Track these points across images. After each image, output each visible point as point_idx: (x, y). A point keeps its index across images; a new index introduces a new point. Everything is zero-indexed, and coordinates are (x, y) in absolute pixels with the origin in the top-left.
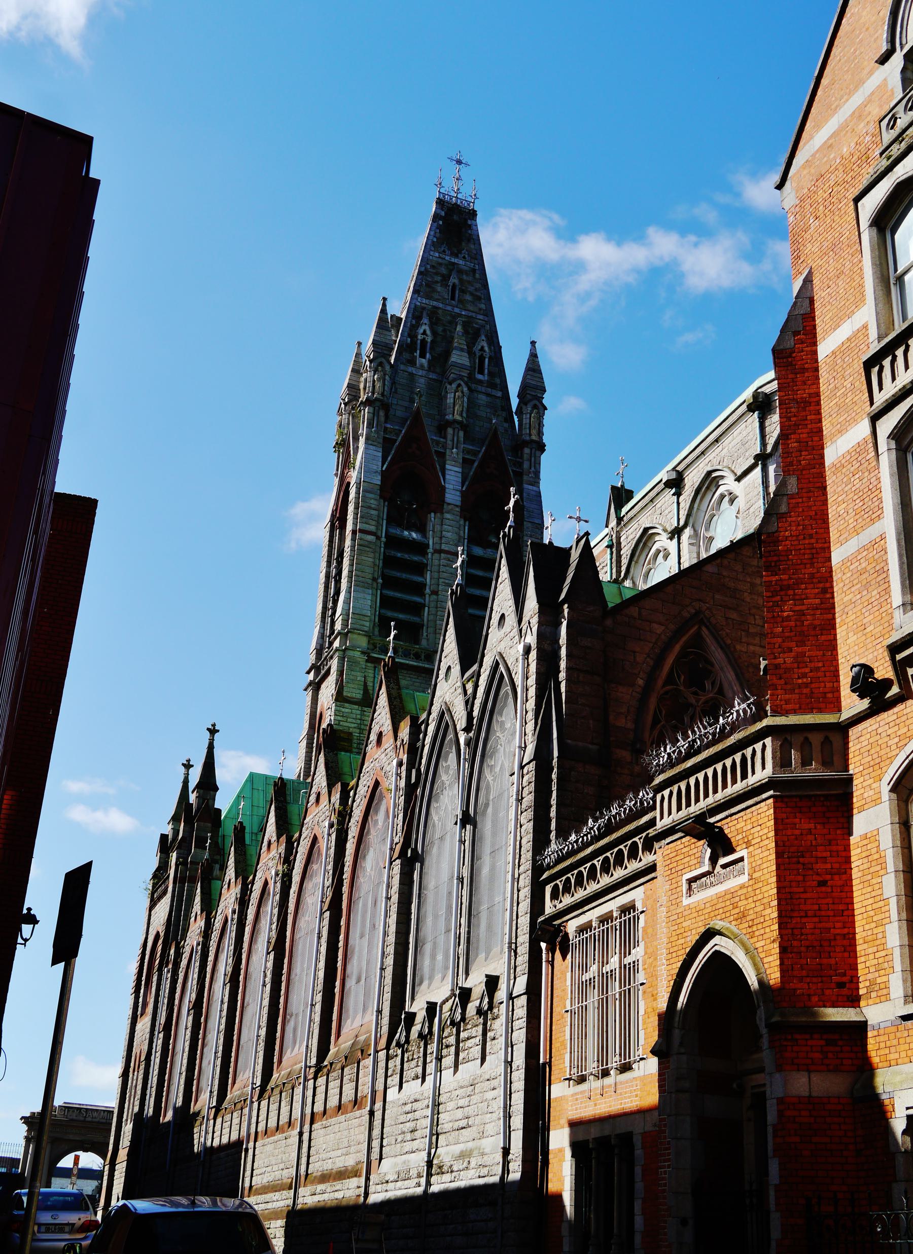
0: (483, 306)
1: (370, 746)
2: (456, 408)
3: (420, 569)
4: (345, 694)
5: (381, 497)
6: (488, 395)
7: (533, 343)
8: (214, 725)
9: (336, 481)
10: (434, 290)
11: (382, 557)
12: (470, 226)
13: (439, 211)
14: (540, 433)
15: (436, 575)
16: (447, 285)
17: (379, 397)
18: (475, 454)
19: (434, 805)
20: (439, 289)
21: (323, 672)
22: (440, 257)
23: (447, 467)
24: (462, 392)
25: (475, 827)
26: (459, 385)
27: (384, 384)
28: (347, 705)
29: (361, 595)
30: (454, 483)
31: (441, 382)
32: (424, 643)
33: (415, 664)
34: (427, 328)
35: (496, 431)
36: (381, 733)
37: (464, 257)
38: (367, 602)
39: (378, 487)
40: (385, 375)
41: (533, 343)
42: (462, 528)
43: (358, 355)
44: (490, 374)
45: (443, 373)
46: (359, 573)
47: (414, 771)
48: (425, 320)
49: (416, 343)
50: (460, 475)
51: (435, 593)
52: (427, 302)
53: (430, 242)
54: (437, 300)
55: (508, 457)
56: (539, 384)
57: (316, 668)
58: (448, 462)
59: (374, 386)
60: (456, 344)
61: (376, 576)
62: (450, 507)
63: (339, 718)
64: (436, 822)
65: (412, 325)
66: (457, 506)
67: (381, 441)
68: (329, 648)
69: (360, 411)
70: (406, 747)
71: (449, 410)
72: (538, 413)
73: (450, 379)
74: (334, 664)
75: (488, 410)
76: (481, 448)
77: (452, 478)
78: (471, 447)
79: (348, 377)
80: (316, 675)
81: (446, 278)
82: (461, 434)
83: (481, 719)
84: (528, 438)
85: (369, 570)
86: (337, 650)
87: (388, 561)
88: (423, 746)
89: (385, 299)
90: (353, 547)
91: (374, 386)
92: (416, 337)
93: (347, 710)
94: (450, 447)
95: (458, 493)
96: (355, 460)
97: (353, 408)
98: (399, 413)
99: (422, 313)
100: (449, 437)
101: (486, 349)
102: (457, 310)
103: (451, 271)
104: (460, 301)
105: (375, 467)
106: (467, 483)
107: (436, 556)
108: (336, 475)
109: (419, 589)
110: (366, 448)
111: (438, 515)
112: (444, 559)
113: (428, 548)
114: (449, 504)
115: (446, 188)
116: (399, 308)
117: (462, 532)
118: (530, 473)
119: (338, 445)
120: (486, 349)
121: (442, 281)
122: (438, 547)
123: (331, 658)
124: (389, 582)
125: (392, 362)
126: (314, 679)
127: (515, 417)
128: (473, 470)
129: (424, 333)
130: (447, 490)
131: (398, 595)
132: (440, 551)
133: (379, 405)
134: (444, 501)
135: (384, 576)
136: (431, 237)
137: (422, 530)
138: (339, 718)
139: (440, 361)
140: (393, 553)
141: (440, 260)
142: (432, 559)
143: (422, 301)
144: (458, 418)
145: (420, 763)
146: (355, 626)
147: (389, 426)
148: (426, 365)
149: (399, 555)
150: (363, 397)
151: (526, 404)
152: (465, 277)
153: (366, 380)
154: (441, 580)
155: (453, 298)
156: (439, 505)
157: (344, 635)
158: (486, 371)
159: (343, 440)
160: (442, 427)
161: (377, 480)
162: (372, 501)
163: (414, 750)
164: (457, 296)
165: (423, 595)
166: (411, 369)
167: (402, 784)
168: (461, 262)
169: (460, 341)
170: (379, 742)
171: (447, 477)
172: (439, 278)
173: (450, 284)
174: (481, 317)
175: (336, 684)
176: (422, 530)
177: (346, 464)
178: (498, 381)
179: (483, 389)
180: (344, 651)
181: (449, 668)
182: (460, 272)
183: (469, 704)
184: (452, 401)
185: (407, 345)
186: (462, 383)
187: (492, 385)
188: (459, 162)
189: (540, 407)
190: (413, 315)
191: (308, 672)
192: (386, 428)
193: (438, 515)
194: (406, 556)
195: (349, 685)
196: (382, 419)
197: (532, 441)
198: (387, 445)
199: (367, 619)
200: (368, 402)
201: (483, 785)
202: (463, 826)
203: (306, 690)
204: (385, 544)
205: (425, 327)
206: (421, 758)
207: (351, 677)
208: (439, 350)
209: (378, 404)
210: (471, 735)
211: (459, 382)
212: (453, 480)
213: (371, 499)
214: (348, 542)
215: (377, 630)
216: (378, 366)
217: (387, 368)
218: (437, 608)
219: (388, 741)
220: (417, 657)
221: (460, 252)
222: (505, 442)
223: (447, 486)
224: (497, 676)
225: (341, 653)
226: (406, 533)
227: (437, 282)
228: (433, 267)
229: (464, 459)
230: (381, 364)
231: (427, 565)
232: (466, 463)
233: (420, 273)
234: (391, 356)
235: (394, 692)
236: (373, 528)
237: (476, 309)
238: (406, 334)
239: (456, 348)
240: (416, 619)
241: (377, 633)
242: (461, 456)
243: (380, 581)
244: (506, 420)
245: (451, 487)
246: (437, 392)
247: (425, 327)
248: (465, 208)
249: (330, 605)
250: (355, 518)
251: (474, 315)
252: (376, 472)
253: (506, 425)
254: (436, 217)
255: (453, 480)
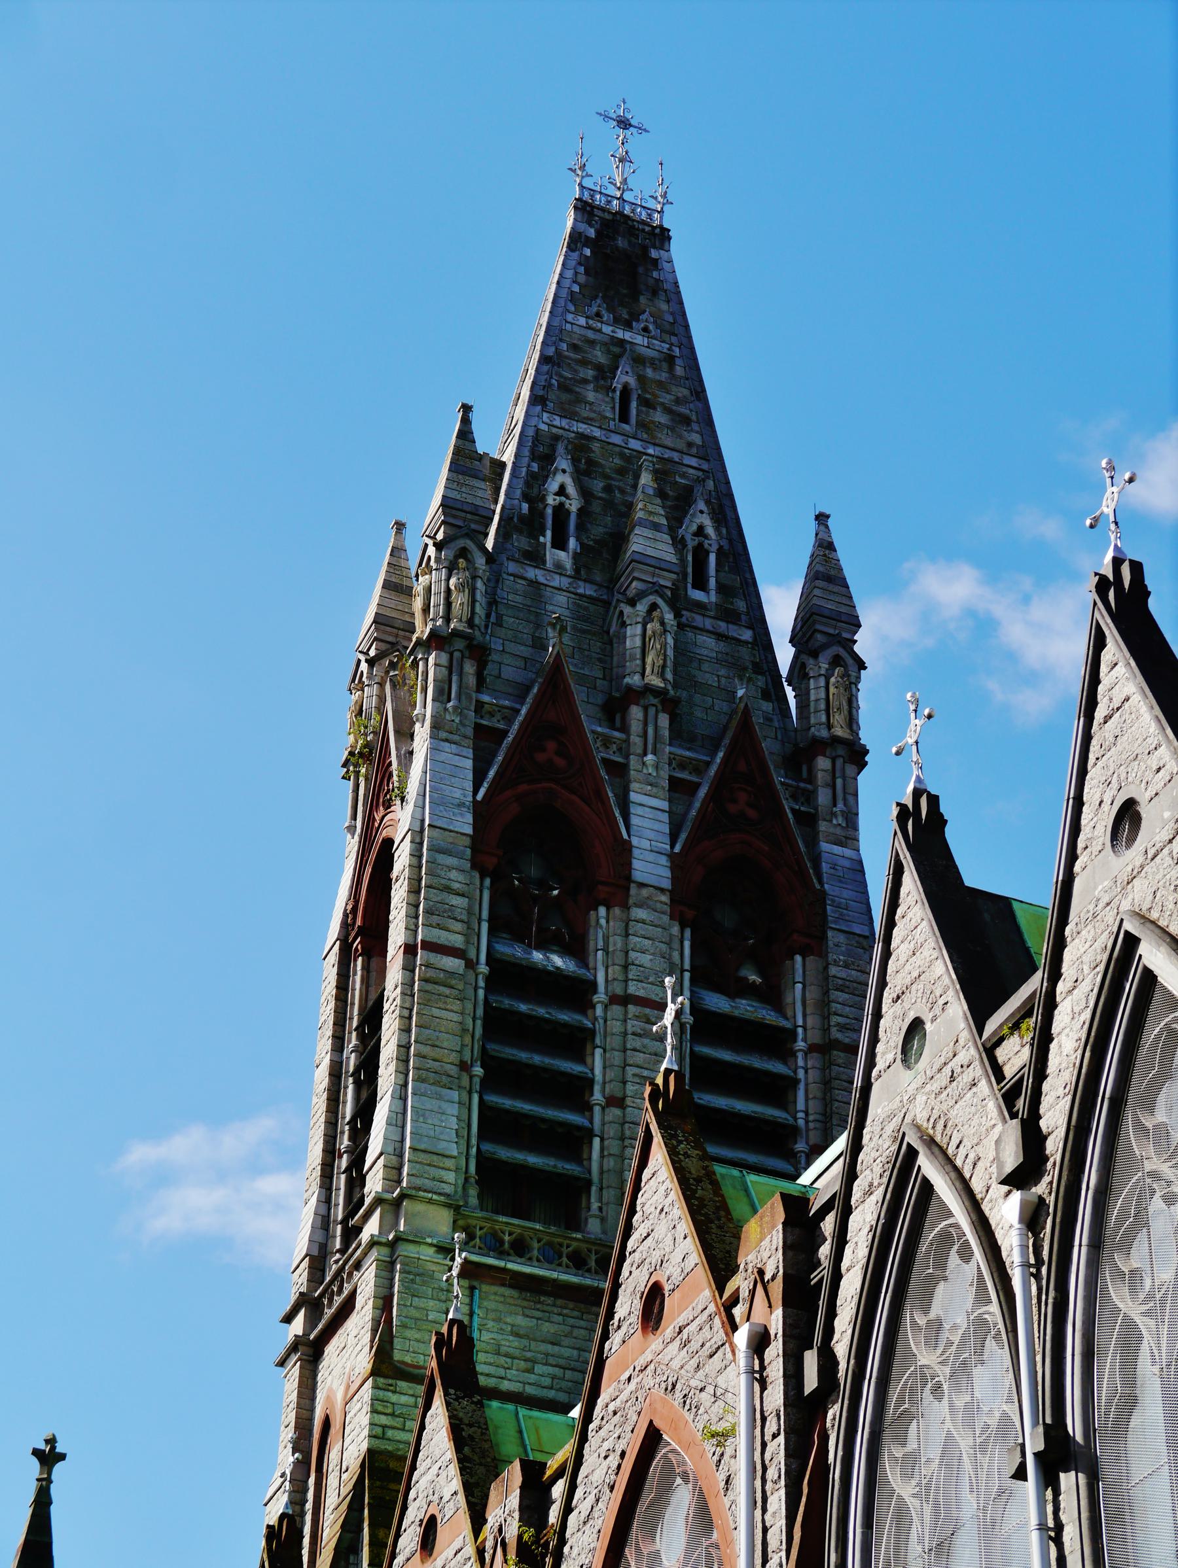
0: (696, 438)
1: (616, 1339)
2: (649, 660)
3: (577, 1042)
4: (397, 1356)
5: (476, 864)
6: (720, 637)
7: (822, 518)
8: (51, 1441)
9: (352, 844)
10: (580, 400)
11: (480, 1012)
12: (655, 262)
13: (582, 227)
14: (852, 722)
15: (617, 1058)
16: (610, 389)
17: (462, 627)
18: (700, 768)
19: (891, 1452)
20: (591, 396)
21: (329, 1313)
22: (589, 327)
23: (633, 796)
24: (663, 623)
25: (1094, 1479)
26: (654, 607)
27: (473, 601)
28: (402, 1385)
29: (430, 1104)
30: (652, 835)
31: (607, 604)
32: (594, 1226)
33: (575, 1279)
34: (568, 481)
35: (747, 712)
36: (433, 1520)
37: (646, 329)
38: (450, 1121)
39: (467, 842)
40: (474, 578)
41: (822, 518)
42: (676, 945)
43: (397, 551)
44: (721, 588)
45: (611, 584)
46: (426, 1050)
47: (811, 1360)
48: (563, 463)
49: (542, 515)
50: (665, 817)
51: (616, 1101)
52: (564, 423)
53: (564, 293)
54: (584, 421)
55: (779, 779)
56: (843, 609)
57: (308, 1303)
58: (634, 786)
59: (448, 604)
60: (640, 514)
61: (467, 1057)
62: (645, 892)
63: (384, 1420)
64: (913, 1503)
65: (532, 476)
66: (662, 890)
67: (470, 731)
68: (343, 1251)
69: (415, 664)
70: (777, 1288)
71: (633, 665)
72: (846, 675)
73: (631, 592)
74: (366, 1282)
75: (722, 672)
76: (713, 754)
77: (647, 823)
78: (688, 754)
79: (375, 600)
80: (311, 1323)
81: (605, 374)
82: (664, 720)
83: (1079, 1131)
84: (824, 733)
85: (450, 1042)
86: (373, 1243)
87: (497, 1024)
88: (837, 1276)
89: (466, 409)
90: (408, 984)
91: (448, 604)
92: (543, 499)
93: (404, 1399)
94: (640, 751)
95: (664, 860)
96: (403, 781)
97: (393, 666)
98: (508, 672)
99: (553, 448)
100: (635, 727)
101: (710, 531)
102: (635, 444)
103: (616, 358)
104: (641, 425)
105: (458, 794)
106: (683, 836)
107: (616, 1010)
108: (351, 829)
109: (575, 1091)
110: (433, 749)
111: (617, 911)
112: (637, 1017)
113: (595, 991)
114: (642, 885)
115: (596, 178)
116: (501, 443)
117: (676, 956)
118: (834, 815)
119: (353, 760)
120: (710, 531)
121: (596, 378)
122: (619, 991)
123: (358, 1266)
124: (499, 1076)
125: (489, 544)
126: (306, 1334)
127: (790, 693)
128: (697, 805)
129: (562, 491)
130: (636, 852)
131: (526, 1107)
132: (625, 1000)
133: (463, 646)
134: (628, 879)
135: (487, 1059)
136: (567, 283)
137: (577, 948)
138: (384, 1420)
139: (604, 555)
140: (507, 1003)
141: (590, 334)
142: (603, 1015)
143: (550, 422)
144: (657, 682)
145: (829, 1331)
146: (418, 1182)
147: (486, 698)
148: (568, 564)
149: (523, 1007)
150: (422, 630)
151: (815, 654)
152: (649, 372)
153: (428, 590)
154: (630, 1071)
155: (624, 417)
156: (618, 886)
157: (392, 1206)
158: (712, 582)
159: (367, 745)
160: (615, 708)
161: (465, 824)
162: (454, 875)
163: (805, 1297)
164: (634, 412)
165: (586, 1108)
166: (532, 573)
167: (775, 1397)
168: (639, 340)
169: (650, 508)
170: (428, 1542)
171: (634, 820)
172: (590, 373)
173: (618, 384)
174: (694, 462)
175: (374, 1331)
176: (577, 948)
177: (380, 794)
178: (741, 605)
179: (708, 623)
180: (392, 1245)
181: (916, 1027)
182: (639, 360)
183: (1020, 1098)
184: (638, 642)
185: (522, 518)
186: (660, 602)
187: (728, 615)
188: (624, 124)
189: (850, 661)
190: (532, 452)
191: (288, 1319)
192: (480, 705)
193: (617, 911)
194: (541, 1011)
195: (409, 1333)
196: (472, 681)
197: (836, 740)
198: (484, 741)
199: (450, 1163)
200: (436, 640)
201: (1109, 1342)
202: (1049, 1480)
203: (282, 1363)
204: (488, 979)
205: (562, 478)
206: (832, 1314)
207: (413, 1313)
208: (597, 531)
209: (460, 644)
210: (1041, 1189)
211: (652, 598)
212: (649, 831)
213: (450, 868)
214: (394, 974)
215: (473, 1192)
216: (457, 557)
217: (480, 561)
218: (622, 1139)
219: (456, 1538)
220: (578, 1262)
221: (635, 316)
222: (769, 746)
223: (635, 841)
224: (911, 1194)
225: (385, 1251)
226: (537, 956)
227: (585, 381)
228: (574, 347)
229: (672, 780)
230: (463, 553)
231: (592, 1033)
232: (679, 789)
233: (544, 359)
234: (486, 535)
235: (693, 1166)
236: (457, 940)
237: (681, 445)
238: (518, 493)
239: (641, 523)
240: (570, 1168)
241: (473, 1201)
242: (665, 774)
243: (478, 1070)
244: (766, 696)
245: (646, 844)
246: (598, 623)
247: (562, 478)
248: (643, 222)
249: (345, 1142)
250: (413, 916)
251: (676, 456)
252: (461, 805)
253: (767, 706)
254: (575, 240)
255: (649, 831)
